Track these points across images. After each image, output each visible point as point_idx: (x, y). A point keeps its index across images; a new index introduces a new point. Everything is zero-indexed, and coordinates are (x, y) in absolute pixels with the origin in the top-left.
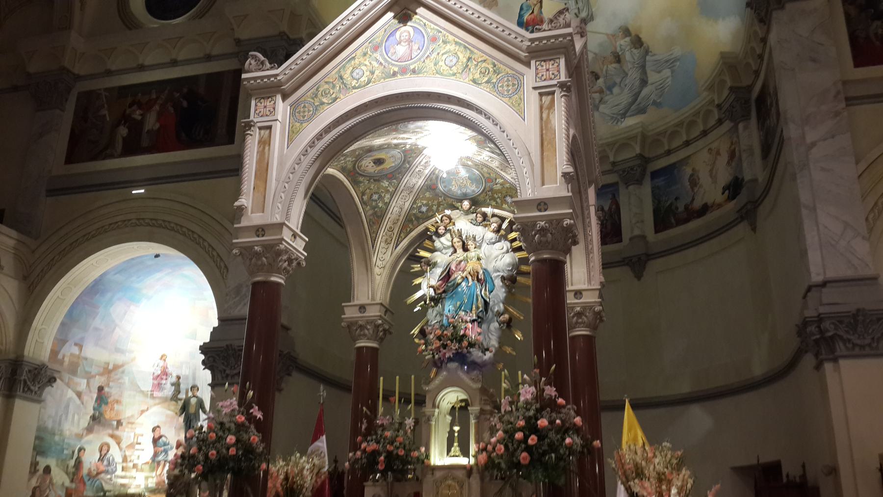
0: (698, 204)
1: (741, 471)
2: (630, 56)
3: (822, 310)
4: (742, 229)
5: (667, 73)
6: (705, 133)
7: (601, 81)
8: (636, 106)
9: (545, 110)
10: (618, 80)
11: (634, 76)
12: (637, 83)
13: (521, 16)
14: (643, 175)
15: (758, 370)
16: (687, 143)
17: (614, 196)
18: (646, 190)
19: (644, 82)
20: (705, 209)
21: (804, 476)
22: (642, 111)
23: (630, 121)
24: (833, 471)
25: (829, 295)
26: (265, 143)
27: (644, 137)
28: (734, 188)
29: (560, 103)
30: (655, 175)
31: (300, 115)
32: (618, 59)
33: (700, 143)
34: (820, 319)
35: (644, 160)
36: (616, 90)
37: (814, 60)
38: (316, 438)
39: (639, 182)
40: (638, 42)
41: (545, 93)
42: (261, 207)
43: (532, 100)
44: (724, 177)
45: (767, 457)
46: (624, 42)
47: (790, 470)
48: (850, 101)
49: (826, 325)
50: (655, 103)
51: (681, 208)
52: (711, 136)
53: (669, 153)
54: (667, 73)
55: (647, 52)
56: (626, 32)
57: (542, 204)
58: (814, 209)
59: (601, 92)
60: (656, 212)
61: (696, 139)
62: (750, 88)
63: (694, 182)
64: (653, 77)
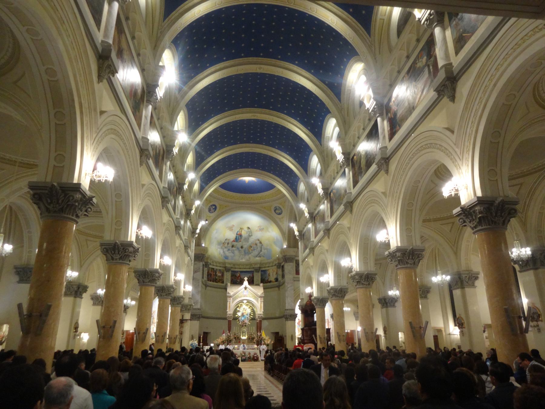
0: (269, 280)
1: (273, 333)
2: (259, 244)
3: (287, 314)
4: (277, 289)
5: (266, 251)
6: (272, 266)
7: (252, 248)
8: (259, 255)
9: (261, 303)
10: (256, 249)
11: (259, 249)
12: (260, 251)
13: (237, 233)
14: (259, 270)
15: (277, 315)
16: (268, 267)
17: (253, 274)
18: (260, 274)
19: (261, 251)
20: (270, 282)
21: (282, 336)
22: (260, 257)
23: (258, 258)
24: (286, 336)
25: (288, 311)
26: (230, 303)
27: (260, 263)
28: (277, 280)
29: (262, 303)
30: (262, 271)
31: (234, 300)
32: (256, 245)
33: (271, 268)
34: (286, 315)
35: (260, 268)
36: (255, 251)
37: (290, 273)
38: (223, 334)
39: (258, 272)
40: (261, 243)
41: (261, 302)
42: (230, 311)
43: (259, 302)
44: (275, 276)
45: (277, 331)
46: (258, 242)
47: (280, 334)
48: (294, 281)
49: (287, 316)
50: (263, 256)
51: (266, 280)
52: (273, 267)
53: (265, 267)
54: (266, 251)
55: (262, 245)
56: (259, 240)
57: (260, 314)
58: (287, 298)
59: (252, 250)
60: (261, 279)
61: (270, 266)
62: (281, 263)
63: (269, 275)
64: (263, 250)
